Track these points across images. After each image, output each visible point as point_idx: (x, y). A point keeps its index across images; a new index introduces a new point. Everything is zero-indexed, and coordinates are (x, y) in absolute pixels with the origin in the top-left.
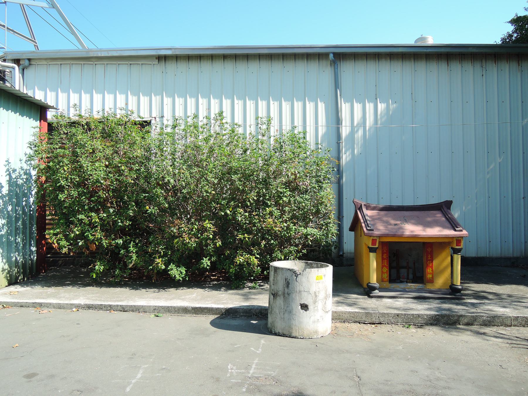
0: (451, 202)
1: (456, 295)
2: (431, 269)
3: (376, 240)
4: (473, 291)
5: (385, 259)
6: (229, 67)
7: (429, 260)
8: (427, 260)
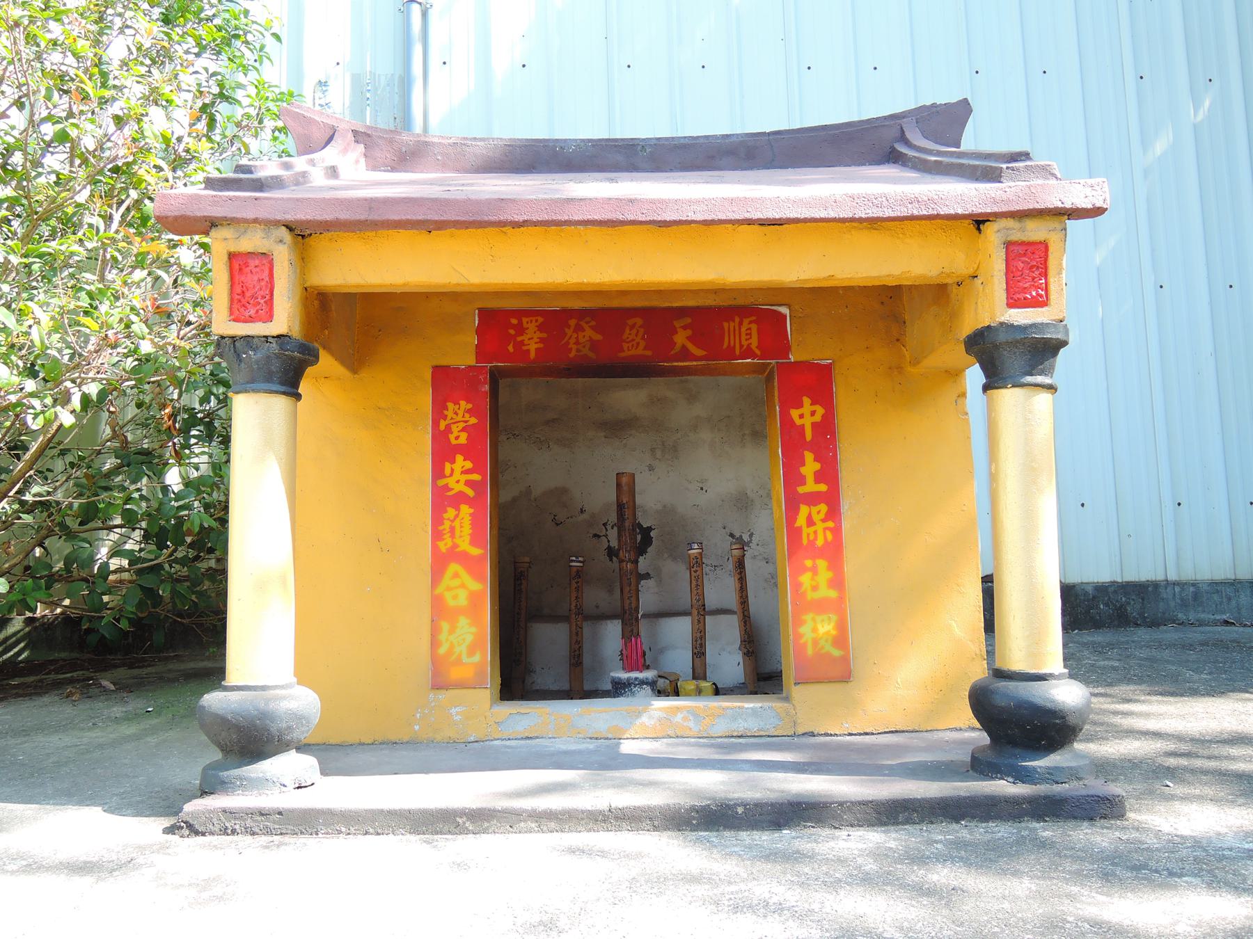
0: (992, 575)
1: (1022, 776)
2: (824, 574)
3: (266, 259)
4: (1157, 735)
5: (460, 499)
6: (420, 238)
7: (812, 499)
8: (793, 502)
